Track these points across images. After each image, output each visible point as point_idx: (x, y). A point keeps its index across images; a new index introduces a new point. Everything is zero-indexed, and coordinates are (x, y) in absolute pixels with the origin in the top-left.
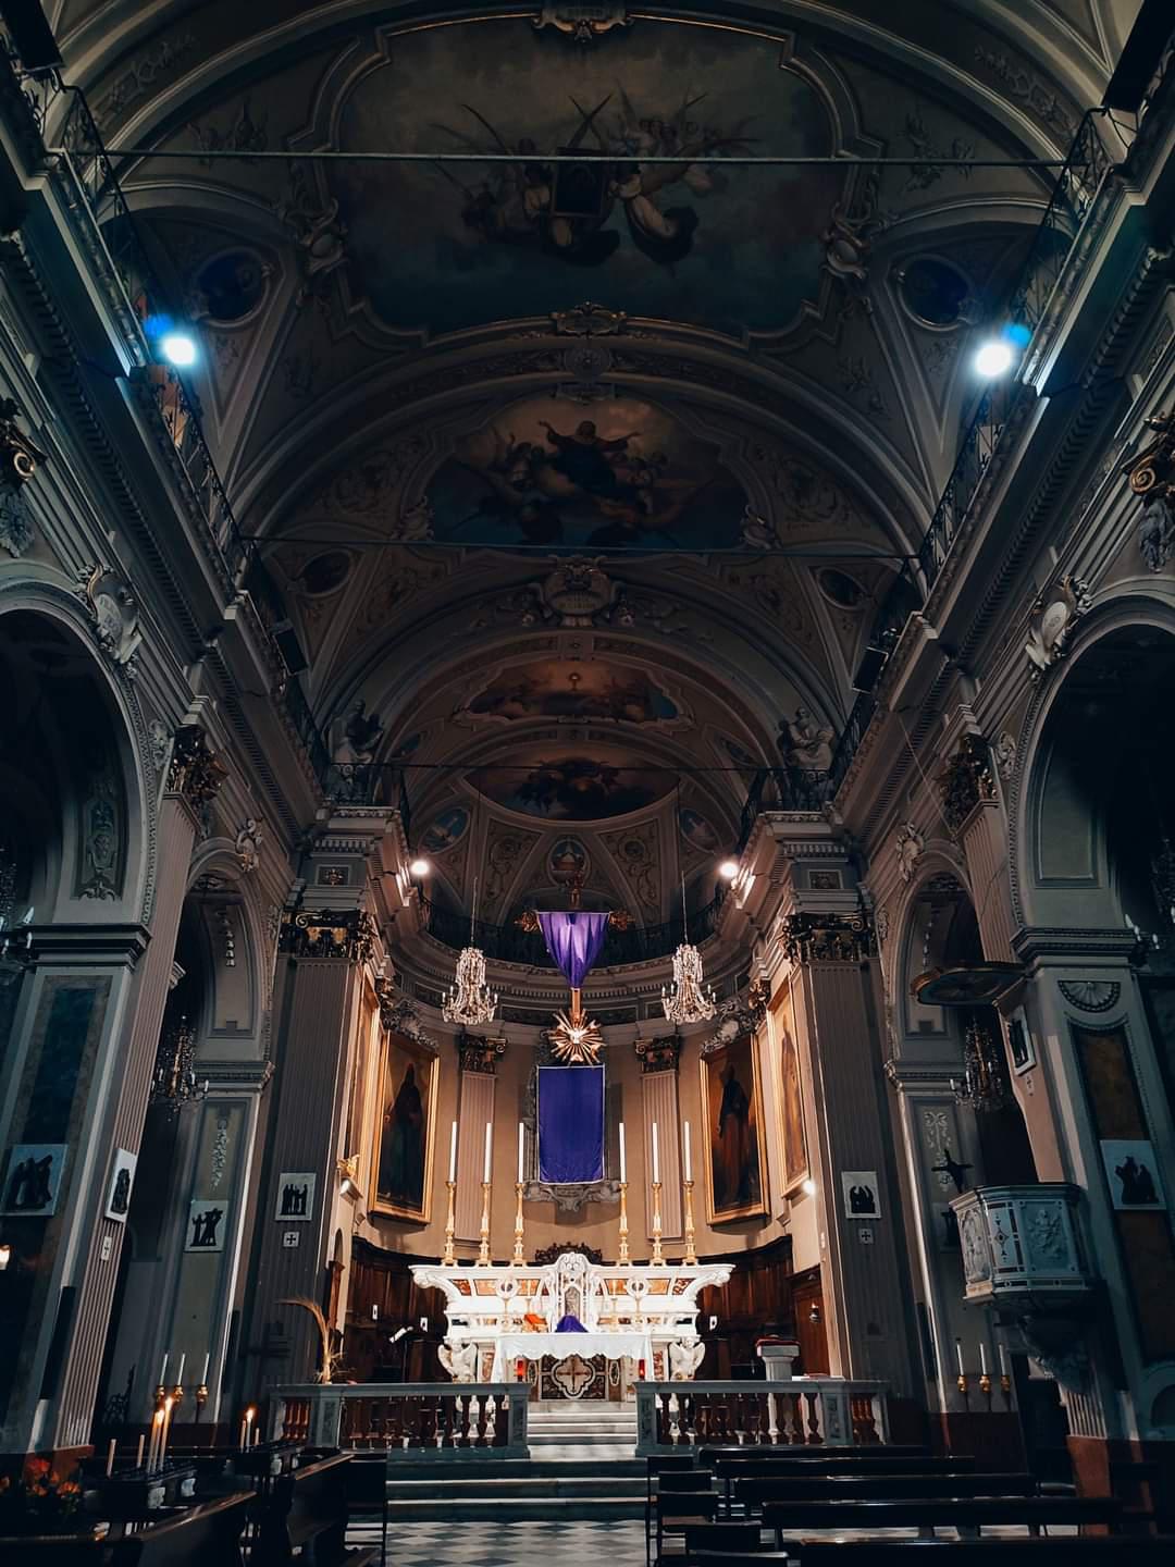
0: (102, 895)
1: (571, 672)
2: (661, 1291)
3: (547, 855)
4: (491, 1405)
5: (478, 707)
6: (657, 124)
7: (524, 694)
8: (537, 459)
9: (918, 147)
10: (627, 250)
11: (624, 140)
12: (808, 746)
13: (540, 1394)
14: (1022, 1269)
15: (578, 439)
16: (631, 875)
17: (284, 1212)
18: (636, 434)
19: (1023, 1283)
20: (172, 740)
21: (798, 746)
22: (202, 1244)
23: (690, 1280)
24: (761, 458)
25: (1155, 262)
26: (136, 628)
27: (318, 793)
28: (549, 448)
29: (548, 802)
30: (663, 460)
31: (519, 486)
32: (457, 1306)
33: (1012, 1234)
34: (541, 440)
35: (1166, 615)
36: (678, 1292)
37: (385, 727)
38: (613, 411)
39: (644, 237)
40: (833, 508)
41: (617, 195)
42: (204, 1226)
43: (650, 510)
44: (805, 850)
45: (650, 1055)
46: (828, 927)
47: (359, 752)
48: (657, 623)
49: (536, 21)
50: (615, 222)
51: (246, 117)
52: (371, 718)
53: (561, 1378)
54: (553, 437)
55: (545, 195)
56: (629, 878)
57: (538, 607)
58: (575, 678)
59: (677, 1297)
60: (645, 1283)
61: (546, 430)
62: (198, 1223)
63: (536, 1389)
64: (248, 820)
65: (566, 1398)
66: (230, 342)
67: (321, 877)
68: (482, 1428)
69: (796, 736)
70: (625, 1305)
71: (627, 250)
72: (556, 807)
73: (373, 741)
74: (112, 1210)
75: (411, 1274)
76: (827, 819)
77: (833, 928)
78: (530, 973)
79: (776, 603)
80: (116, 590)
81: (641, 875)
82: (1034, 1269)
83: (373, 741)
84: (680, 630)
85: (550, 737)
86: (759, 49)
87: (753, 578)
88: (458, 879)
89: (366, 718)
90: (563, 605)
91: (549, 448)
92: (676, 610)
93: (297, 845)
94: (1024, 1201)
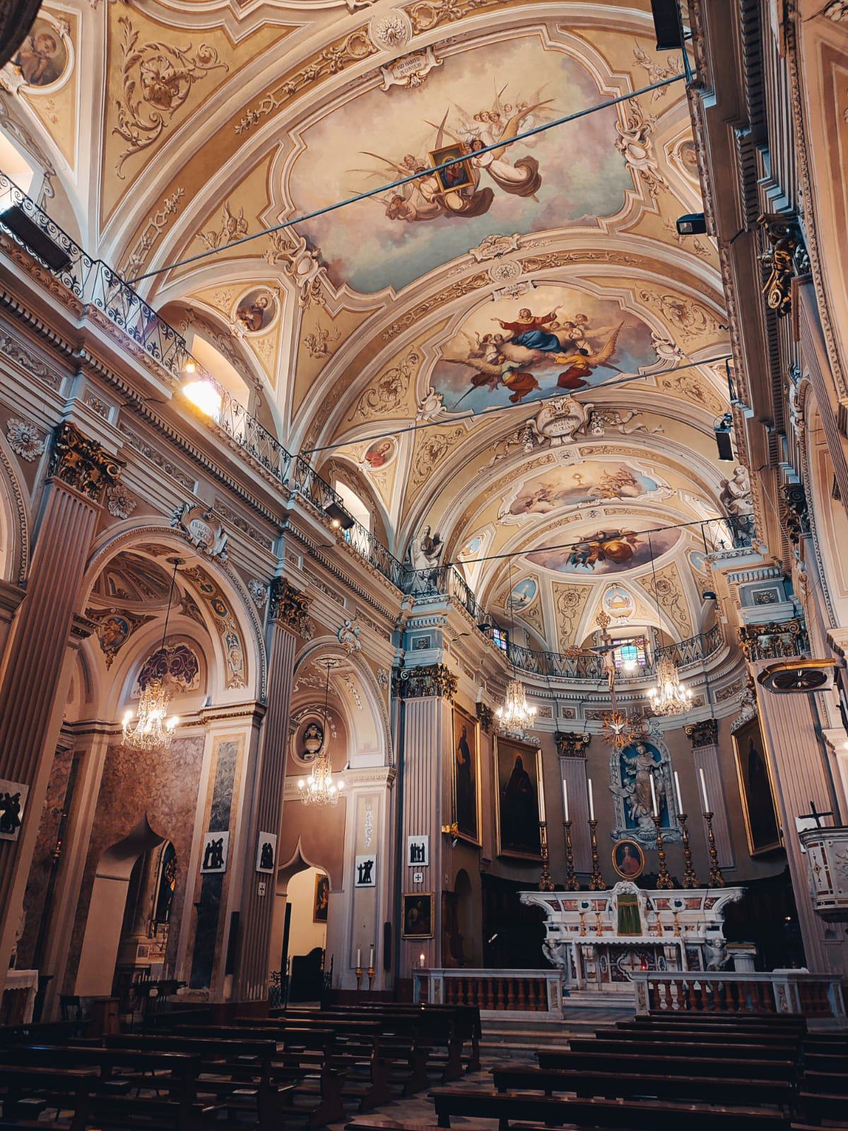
0: (238, 686)
1: (573, 474)
2: (696, 907)
4: (674, 989)
5: (516, 511)
6: (485, 114)
7: (544, 496)
8: (500, 344)
9: (648, 69)
10: (501, 196)
11: (469, 132)
12: (745, 496)
13: (610, 978)
14: (832, 892)
15: (522, 322)
17: (412, 861)
18: (559, 307)
19: (832, 903)
20: (269, 588)
21: (738, 497)
22: (364, 882)
23: (717, 899)
24: (648, 300)
25: (741, 138)
26: (223, 532)
27: (398, 593)
28: (507, 334)
29: (592, 562)
30: (585, 318)
31: (495, 362)
32: (555, 917)
33: (823, 866)
34: (497, 330)
36: (708, 907)
37: (444, 540)
38: (537, 297)
39: (510, 186)
40: (705, 322)
41: (479, 166)
42: (364, 871)
43: (590, 353)
45: (696, 735)
46: (772, 633)
47: (430, 560)
48: (620, 428)
49: (383, 86)
50: (485, 182)
51: (230, 216)
52: (435, 536)
53: (624, 968)
54: (506, 326)
55: (432, 184)
56: (664, 607)
57: (533, 436)
58: (577, 477)
59: (706, 911)
60: (683, 902)
61: (498, 322)
62: (360, 869)
63: (607, 975)
64: (345, 621)
65: (628, 981)
66: (266, 342)
67: (414, 644)
68: (669, 1002)
70: (666, 917)
71: (501, 196)
72: (599, 565)
73: (437, 552)
74: (261, 866)
75: (519, 896)
76: (755, 552)
77: (775, 633)
78: (599, 685)
79: (699, 395)
80: (202, 516)
82: (840, 892)
83: (437, 552)
84: (639, 429)
86: (527, 44)
87: (679, 380)
88: (539, 626)
89: (432, 537)
90: (551, 431)
91: (507, 334)
92: (633, 415)
93: (396, 627)
94: (831, 841)
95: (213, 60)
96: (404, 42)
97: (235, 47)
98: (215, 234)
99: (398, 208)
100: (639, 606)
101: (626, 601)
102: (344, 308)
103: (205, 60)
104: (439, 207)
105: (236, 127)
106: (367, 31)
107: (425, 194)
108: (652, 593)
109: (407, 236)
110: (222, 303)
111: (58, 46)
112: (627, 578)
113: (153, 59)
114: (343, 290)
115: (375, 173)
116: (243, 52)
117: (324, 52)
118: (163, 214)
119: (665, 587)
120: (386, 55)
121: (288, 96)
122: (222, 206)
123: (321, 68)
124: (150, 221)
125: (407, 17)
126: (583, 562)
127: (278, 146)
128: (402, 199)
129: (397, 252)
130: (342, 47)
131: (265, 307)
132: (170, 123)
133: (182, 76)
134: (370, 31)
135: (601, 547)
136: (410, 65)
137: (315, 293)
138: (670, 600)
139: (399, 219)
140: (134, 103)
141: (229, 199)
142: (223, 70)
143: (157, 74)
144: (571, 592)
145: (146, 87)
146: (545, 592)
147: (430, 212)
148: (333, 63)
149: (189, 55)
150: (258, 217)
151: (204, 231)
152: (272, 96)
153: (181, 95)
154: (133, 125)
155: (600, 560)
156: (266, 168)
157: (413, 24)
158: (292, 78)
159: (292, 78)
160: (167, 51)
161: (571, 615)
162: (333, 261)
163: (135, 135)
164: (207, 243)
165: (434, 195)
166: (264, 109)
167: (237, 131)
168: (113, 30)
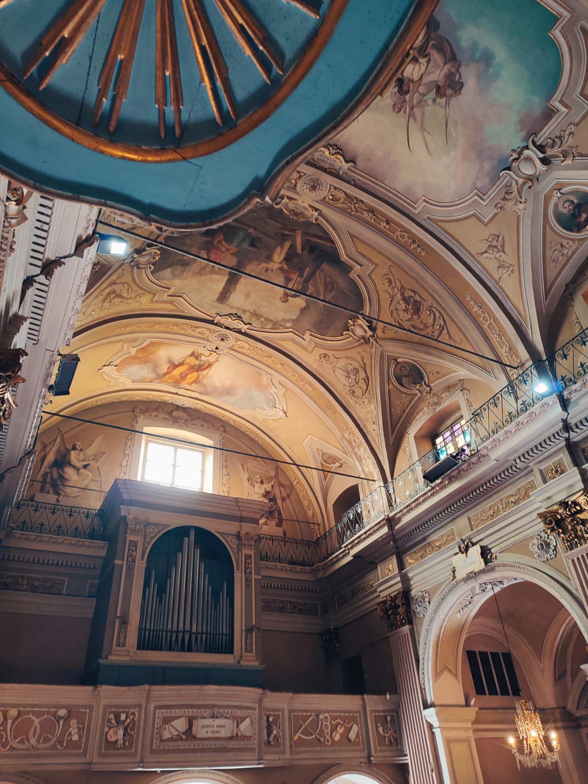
51: (486, 252)
95: (388, 277)
96: (313, 177)
97: (377, 265)
98: (499, 267)
99: (449, 87)
102: (582, 94)
103: (390, 282)
104: (431, 44)
105: (423, 254)
106: (325, 198)
107: (423, 69)
109: (477, 56)
110: (565, 252)
111: (405, 365)
113: (397, 313)
114: (557, 104)
115: (423, 129)
116: (377, 259)
117: (353, 213)
118: (482, 315)
120: (328, 180)
121: (392, 224)
122: (478, 259)
123: (364, 210)
124: (485, 327)
125: (298, 184)
127: (428, 218)
128: (438, 88)
129: (501, 54)
130: (343, 205)
131: (572, 202)
132: (430, 301)
133: (402, 294)
134: (323, 196)
136: (326, 160)
137: (559, 144)
139: (460, 77)
140: (422, 326)
141: (474, 253)
142: (391, 268)
143: (404, 310)
145: (412, 318)
147: (440, 49)
148: (356, 205)
149: (390, 291)
150: (486, 225)
151: (497, 277)
152: (396, 235)
153: (413, 295)
154: (433, 328)
156: (447, 224)
157: (299, 179)
158: (379, 225)
159: (379, 225)
160: (392, 305)
162: (522, 130)
163: (438, 327)
164: (505, 275)
165: (421, 60)
166: (406, 237)
167: (425, 254)
168: (389, 337)
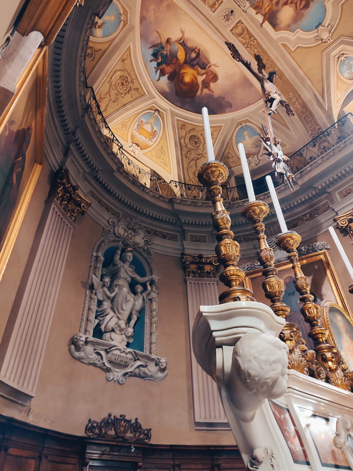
3: (337, 73)
16: (186, 157)
29: (163, 73)
35: (288, 77)
44: (299, 202)
56: (184, 158)
69: (341, 138)
81: (193, 160)
85: (245, 30)
100: (160, 147)
101: (154, 134)
108: (182, 141)
112: (173, 114)
119: (196, 143)
126: (159, 64)
135: (181, 67)
138: (193, 155)
144: (129, 79)
146: (117, 47)
155: (169, 78)
161: (113, 98)
